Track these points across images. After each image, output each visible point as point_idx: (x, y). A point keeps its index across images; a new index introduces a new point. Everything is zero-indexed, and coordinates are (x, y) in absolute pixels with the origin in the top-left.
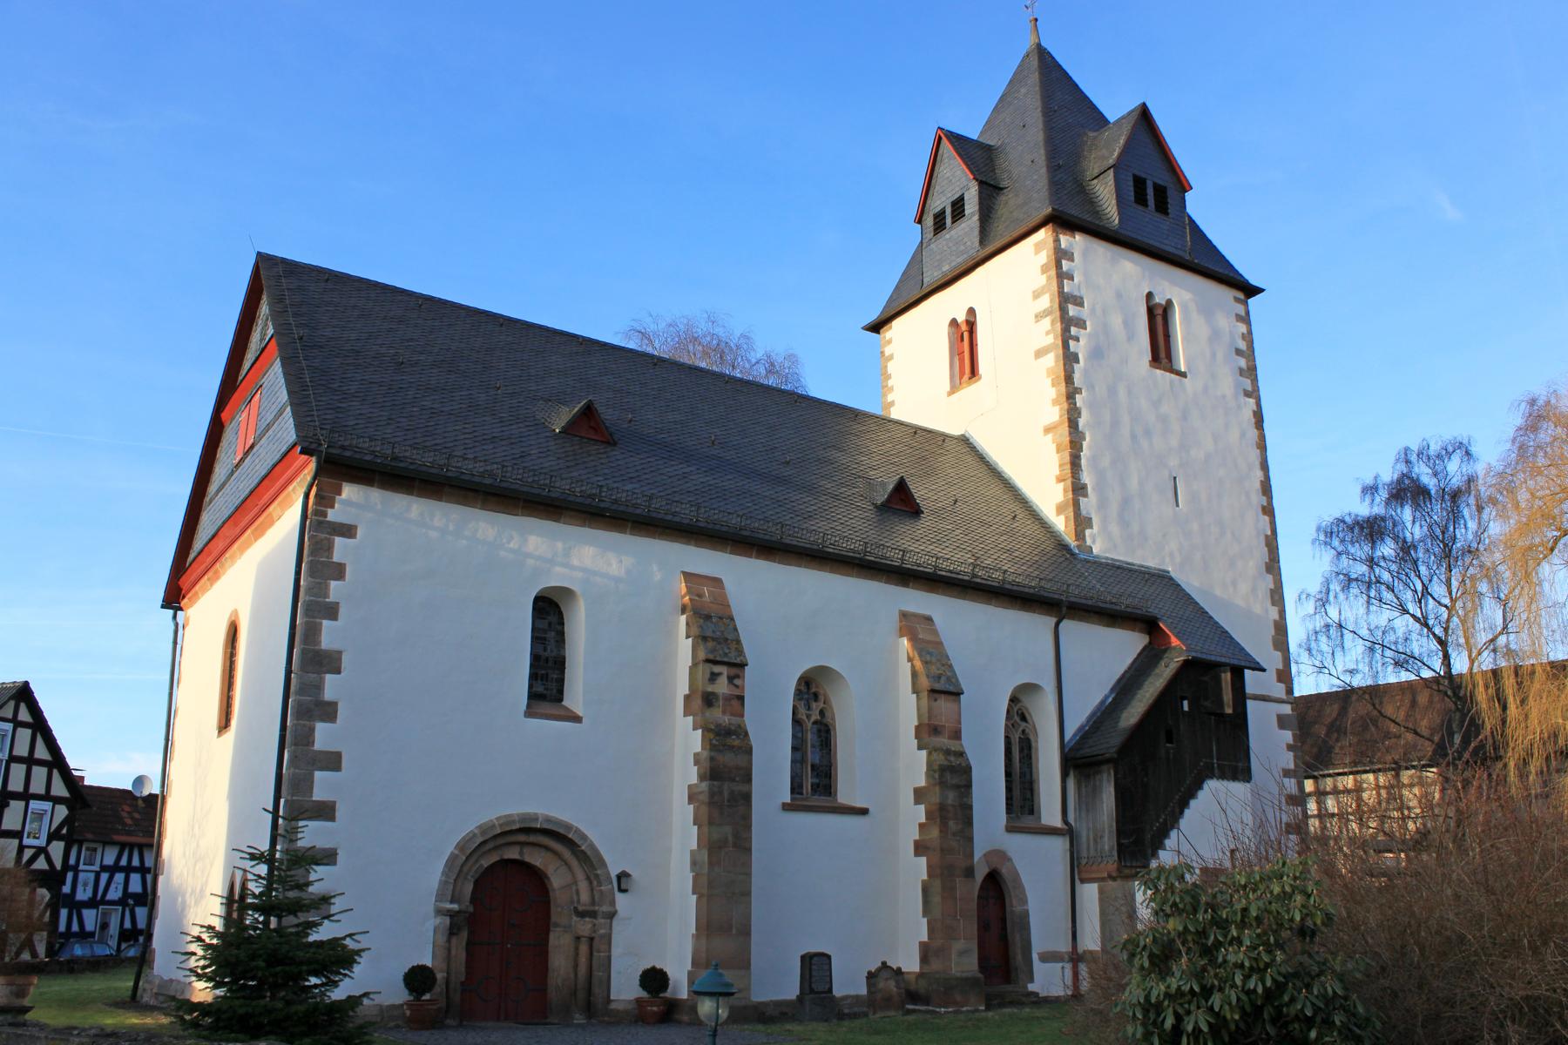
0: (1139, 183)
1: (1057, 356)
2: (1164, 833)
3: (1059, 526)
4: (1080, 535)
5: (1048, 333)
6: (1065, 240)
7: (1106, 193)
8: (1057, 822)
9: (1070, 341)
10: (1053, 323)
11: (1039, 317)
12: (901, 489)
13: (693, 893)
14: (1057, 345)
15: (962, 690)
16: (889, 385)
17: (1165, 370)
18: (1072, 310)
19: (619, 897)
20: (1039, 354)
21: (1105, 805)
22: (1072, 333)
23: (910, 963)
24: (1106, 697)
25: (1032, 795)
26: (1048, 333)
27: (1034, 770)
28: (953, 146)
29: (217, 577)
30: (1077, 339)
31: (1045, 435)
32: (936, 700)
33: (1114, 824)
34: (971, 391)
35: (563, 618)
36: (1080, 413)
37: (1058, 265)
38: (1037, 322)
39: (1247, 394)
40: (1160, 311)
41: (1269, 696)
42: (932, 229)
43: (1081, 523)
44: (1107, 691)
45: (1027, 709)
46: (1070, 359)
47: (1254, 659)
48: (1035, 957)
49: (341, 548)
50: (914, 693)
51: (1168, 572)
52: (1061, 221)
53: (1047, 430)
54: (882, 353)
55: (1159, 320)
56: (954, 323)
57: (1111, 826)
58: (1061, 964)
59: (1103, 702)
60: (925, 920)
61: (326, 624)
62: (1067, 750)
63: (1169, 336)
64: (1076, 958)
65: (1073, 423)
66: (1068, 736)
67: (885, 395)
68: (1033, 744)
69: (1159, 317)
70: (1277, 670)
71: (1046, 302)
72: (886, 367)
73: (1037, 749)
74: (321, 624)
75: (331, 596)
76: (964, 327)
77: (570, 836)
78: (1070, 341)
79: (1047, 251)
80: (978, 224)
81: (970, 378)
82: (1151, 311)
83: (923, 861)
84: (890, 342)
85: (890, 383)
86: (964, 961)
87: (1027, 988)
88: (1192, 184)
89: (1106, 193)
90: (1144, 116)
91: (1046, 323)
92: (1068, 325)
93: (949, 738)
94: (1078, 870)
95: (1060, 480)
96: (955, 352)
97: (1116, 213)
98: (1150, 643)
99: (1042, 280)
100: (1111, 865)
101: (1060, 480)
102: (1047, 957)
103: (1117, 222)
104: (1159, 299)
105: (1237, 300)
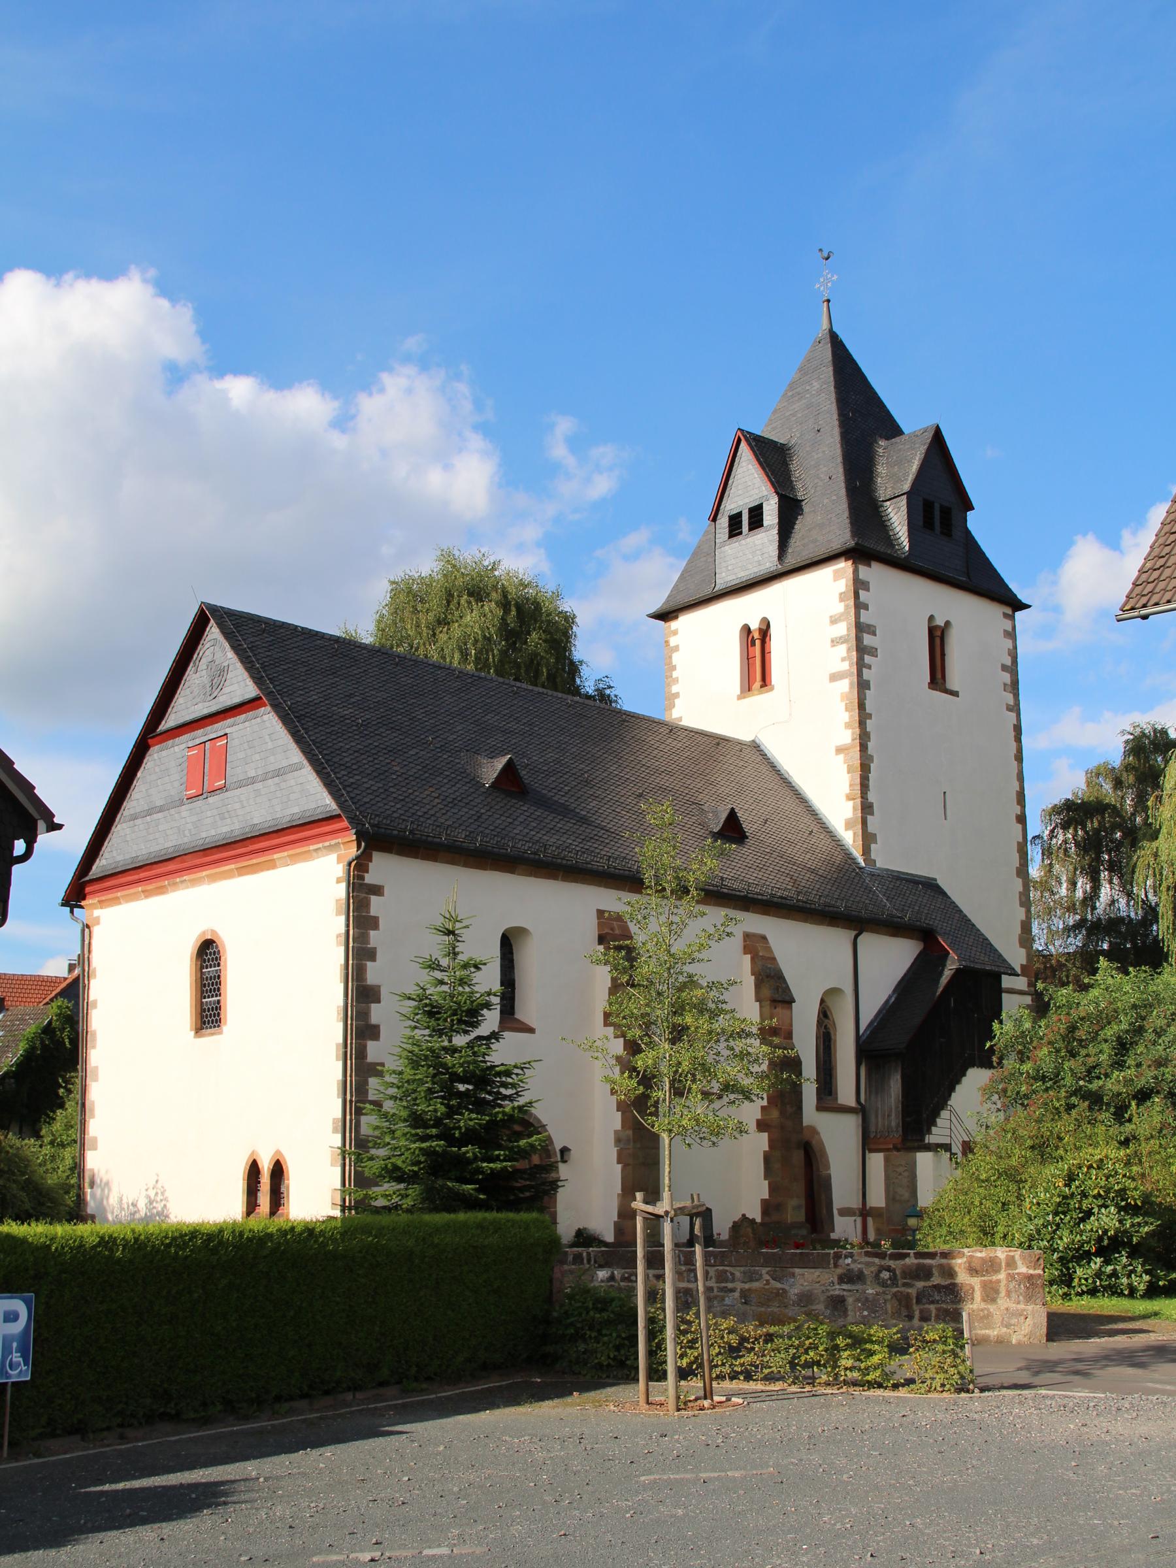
0: (928, 506)
1: (851, 684)
2: (935, 1114)
3: (847, 839)
4: (866, 851)
5: (843, 660)
6: (863, 571)
7: (898, 518)
8: (852, 1103)
9: (864, 669)
10: (849, 650)
11: (835, 642)
12: (732, 816)
13: (618, 1163)
14: (853, 673)
15: (793, 998)
16: (674, 676)
17: (941, 691)
18: (868, 640)
19: (561, 1166)
20: (834, 677)
21: (892, 1089)
22: (866, 661)
23: (756, 1214)
24: (890, 997)
25: (831, 1078)
26: (843, 660)
27: (833, 1059)
28: (752, 448)
29: (161, 891)
30: (869, 667)
31: (837, 754)
32: (775, 1008)
33: (900, 1106)
34: (759, 700)
35: (512, 949)
36: (869, 738)
37: (856, 595)
38: (833, 646)
39: (1009, 709)
40: (939, 633)
41: (1012, 989)
42: (727, 530)
43: (868, 839)
44: (890, 991)
45: (828, 1007)
46: (863, 686)
47: (1010, 965)
48: (835, 1212)
49: (376, 905)
50: (757, 1001)
51: (936, 880)
52: (858, 554)
53: (839, 750)
54: (667, 642)
55: (938, 641)
56: (747, 630)
57: (897, 1107)
58: (854, 1218)
59: (887, 1001)
60: (767, 1182)
61: (369, 964)
62: (861, 1042)
63: (944, 655)
64: (865, 1212)
65: (863, 747)
66: (861, 1032)
67: (669, 685)
68: (833, 1037)
69: (937, 637)
70: (1021, 965)
71: (844, 629)
72: (670, 657)
73: (835, 1041)
74: (366, 964)
75: (371, 942)
76: (756, 635)
77: (531, 1121)
78: (864, 669)
79: (847, 580)
80: (776, 537)
81: (761, 687)
82: (932, 631)
83: (765, 1135)
84: (675, 633)
85: (675, 674)
86: (794, 1211)
87: (829, 1236)
88: (974, 504)
89: (898, 518)
90: (938, 441)
91: (842, 650)
92: (862, 651)
93: (785, 1038)
94: (868, 1143)
95: (849, 798)
96: (747, 659)
97: (907, 540)
98: (924, 948)
99: (840, 608)
100: (897, 1136)
101: (849, 798)
102: (845, 1212)
103: (907, 548)
104: (940, 622)
105: (1006, 615)
